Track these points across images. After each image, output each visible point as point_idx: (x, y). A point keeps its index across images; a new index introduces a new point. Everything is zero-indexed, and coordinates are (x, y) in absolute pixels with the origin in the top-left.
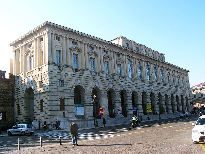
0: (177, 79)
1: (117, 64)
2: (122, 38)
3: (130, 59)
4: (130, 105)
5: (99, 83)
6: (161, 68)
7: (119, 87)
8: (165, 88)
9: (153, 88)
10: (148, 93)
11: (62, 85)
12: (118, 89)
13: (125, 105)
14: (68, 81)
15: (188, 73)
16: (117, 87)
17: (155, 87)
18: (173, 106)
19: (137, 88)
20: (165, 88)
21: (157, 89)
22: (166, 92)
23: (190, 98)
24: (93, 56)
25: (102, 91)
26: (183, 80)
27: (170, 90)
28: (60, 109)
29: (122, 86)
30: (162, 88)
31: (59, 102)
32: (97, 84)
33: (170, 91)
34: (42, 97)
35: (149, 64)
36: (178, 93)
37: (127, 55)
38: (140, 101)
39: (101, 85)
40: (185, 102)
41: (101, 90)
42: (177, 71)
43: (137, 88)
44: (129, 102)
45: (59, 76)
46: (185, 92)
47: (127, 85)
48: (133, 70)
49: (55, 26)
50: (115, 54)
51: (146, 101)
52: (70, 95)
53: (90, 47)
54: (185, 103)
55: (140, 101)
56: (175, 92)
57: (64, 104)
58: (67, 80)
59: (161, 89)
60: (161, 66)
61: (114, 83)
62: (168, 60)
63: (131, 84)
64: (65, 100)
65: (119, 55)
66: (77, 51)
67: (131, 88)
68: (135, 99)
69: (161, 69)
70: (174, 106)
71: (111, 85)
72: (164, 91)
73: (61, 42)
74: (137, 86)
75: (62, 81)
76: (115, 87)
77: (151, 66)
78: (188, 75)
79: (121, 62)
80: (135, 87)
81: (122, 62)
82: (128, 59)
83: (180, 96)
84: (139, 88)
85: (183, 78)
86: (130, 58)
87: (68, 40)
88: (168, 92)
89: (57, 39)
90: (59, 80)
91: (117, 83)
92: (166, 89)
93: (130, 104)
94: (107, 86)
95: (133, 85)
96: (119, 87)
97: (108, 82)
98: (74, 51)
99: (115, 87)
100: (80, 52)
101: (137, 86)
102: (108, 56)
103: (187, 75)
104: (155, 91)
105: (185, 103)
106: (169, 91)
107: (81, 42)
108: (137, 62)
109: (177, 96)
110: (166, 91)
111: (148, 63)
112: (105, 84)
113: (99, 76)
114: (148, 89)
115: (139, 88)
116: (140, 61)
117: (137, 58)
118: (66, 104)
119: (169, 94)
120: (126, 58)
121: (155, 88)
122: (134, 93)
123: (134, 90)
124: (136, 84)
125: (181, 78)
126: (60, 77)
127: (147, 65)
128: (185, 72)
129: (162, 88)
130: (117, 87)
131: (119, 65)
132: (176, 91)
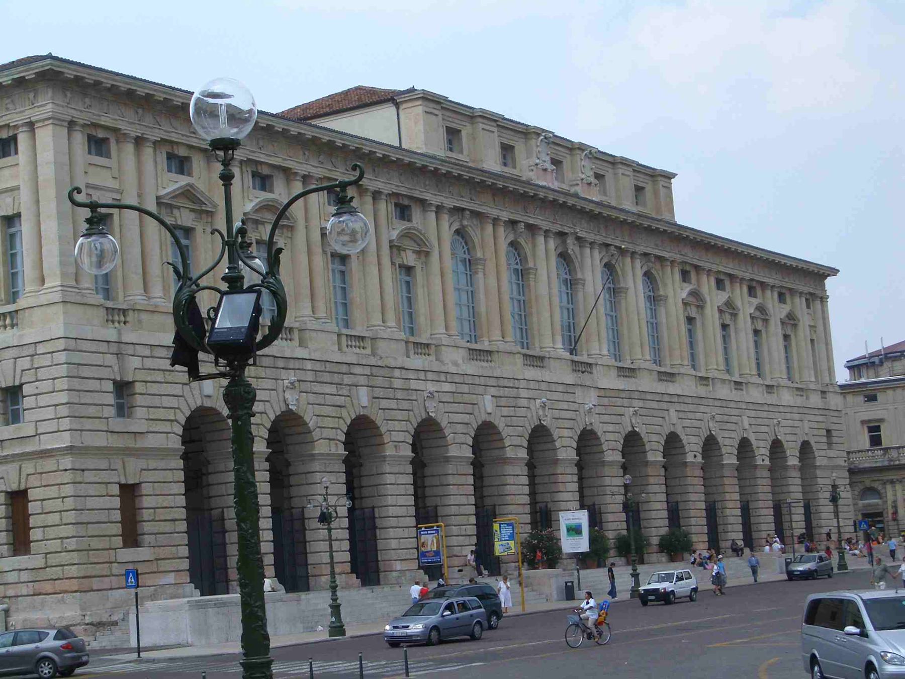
0: (718, 324)
1: (393, 263)
2: (423, 98)
3: (464, 227)
4: (463, 510)
5: (304, 386)
6: (645, 269)
7: (405, 405)
8: (666, 398)
9: (591, 399)
10: (566, 433)
11: (123, 410)
12: (399, 415)
13: (215, 513)
14: (154, 389)
15: (829, 282)
16: (393, 404)
17: (604, 393)
18: (677, 510)
19: (503, 402)
20: (666, 398)
21: (619, 402)
22: (673, 420)
23: (831, 453)
24: (409, 253)
25: (316, 434)
26: (789, 332)
27: (702, 409)
28: (118, 541)
29: (420, 401)
30: (649, 397)
31: (117, 502)
32: (431, 406)
33: (698, 416)
34: (23, 476)
35: (572, 246)
36: (753, 421)
37: (450, 203)
38: (515, 487)
39: (312, 398)
40: (799, 481)
41: (311, 425)
42: (679, 258)
43: (503, 402)
44: (452, 489)
45: (111, 360)
46: (797, 417)
47: (447, 387)
48: (482, 296)
49: (90, 78)
50: (382, 206)
51: (552, 479)
52: (162, 464)
53: (170, 157)
54: (795, 491)
55: (515, 487)
56: (734, 419)
57: (134, 515)
58: (149, 379)
59: (641, 404)
60: (646, 255)
61: (379, 381)
62: (690, 210)
63: (469, 380)
64: (146, 489)
65: (403, 212)
66: (192, 210)
67: (469, 408)
68: (486, 471)
69: (514, 244)
70: (719, 513)
71: (363, 396)
72: (660, 414)
73: (112, 162)
74: (501, 392)
75: (123, 388)
76: (384, 404)
77: (588, 261)
78: (823, 299)
79: (414, 252)
80: (488, 398)
81: (418, 253)
82: (456, 226)
83: (762, 444)
84: (511, 402)
85: (791, 320)
86: (465, 223)
87: (148, 151)
88: (687, 423)
89: (93, 151)
90: (115, 382)
91: (397, 383)
92: (675, 399)
93: (463, 500)
94: (340, 400)
95: (480, 390)
96: (405, 405)
97: (347, 380)
98: (179, 208)
99: (384, 404)
100: (204, 216)
101: (501, 392)
102: (188, 194)
103: (817, 298)
104: (606, 418)
105: (795, 491)
106: (690, 415)
107: (423, 203)
108: (504, 237)
109: (744, 446)
110: (673, 413)
111: (570, 241)
112: (331, 389)
113: (302, 344)
114: (565, 406)
115: (511, 402)
116: (521, 236)
117: (505, 216)
118: (146, 514)
119: (688, 431)
120: (445, 224)
121: (606, 401)
122: (485, 436)
123: (484, 417)
124: (492, 382)
125: (741, 316)
126: (116, 368)
127: (564, 256)
128: (817, 275)
129: (649, 397)
130: (393, 404)
131: (337, 260)
132: (736, 412)
